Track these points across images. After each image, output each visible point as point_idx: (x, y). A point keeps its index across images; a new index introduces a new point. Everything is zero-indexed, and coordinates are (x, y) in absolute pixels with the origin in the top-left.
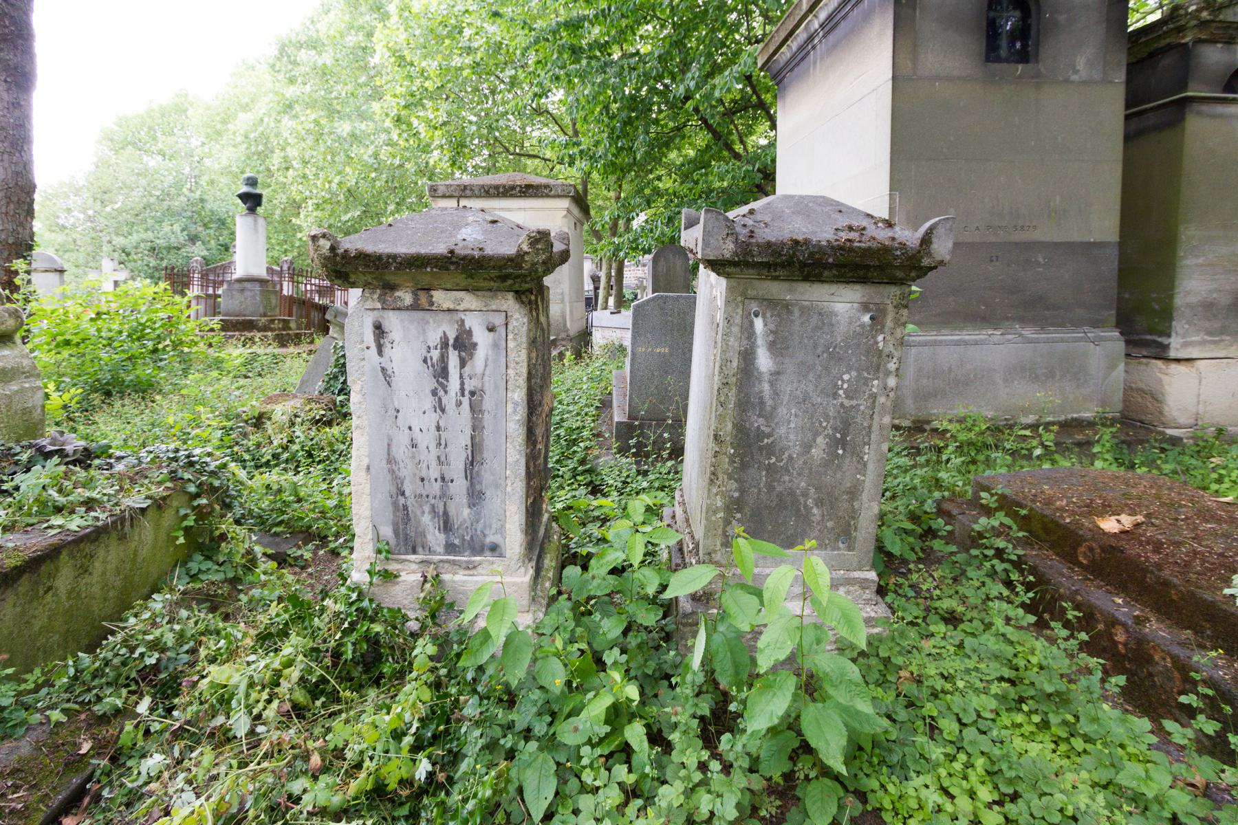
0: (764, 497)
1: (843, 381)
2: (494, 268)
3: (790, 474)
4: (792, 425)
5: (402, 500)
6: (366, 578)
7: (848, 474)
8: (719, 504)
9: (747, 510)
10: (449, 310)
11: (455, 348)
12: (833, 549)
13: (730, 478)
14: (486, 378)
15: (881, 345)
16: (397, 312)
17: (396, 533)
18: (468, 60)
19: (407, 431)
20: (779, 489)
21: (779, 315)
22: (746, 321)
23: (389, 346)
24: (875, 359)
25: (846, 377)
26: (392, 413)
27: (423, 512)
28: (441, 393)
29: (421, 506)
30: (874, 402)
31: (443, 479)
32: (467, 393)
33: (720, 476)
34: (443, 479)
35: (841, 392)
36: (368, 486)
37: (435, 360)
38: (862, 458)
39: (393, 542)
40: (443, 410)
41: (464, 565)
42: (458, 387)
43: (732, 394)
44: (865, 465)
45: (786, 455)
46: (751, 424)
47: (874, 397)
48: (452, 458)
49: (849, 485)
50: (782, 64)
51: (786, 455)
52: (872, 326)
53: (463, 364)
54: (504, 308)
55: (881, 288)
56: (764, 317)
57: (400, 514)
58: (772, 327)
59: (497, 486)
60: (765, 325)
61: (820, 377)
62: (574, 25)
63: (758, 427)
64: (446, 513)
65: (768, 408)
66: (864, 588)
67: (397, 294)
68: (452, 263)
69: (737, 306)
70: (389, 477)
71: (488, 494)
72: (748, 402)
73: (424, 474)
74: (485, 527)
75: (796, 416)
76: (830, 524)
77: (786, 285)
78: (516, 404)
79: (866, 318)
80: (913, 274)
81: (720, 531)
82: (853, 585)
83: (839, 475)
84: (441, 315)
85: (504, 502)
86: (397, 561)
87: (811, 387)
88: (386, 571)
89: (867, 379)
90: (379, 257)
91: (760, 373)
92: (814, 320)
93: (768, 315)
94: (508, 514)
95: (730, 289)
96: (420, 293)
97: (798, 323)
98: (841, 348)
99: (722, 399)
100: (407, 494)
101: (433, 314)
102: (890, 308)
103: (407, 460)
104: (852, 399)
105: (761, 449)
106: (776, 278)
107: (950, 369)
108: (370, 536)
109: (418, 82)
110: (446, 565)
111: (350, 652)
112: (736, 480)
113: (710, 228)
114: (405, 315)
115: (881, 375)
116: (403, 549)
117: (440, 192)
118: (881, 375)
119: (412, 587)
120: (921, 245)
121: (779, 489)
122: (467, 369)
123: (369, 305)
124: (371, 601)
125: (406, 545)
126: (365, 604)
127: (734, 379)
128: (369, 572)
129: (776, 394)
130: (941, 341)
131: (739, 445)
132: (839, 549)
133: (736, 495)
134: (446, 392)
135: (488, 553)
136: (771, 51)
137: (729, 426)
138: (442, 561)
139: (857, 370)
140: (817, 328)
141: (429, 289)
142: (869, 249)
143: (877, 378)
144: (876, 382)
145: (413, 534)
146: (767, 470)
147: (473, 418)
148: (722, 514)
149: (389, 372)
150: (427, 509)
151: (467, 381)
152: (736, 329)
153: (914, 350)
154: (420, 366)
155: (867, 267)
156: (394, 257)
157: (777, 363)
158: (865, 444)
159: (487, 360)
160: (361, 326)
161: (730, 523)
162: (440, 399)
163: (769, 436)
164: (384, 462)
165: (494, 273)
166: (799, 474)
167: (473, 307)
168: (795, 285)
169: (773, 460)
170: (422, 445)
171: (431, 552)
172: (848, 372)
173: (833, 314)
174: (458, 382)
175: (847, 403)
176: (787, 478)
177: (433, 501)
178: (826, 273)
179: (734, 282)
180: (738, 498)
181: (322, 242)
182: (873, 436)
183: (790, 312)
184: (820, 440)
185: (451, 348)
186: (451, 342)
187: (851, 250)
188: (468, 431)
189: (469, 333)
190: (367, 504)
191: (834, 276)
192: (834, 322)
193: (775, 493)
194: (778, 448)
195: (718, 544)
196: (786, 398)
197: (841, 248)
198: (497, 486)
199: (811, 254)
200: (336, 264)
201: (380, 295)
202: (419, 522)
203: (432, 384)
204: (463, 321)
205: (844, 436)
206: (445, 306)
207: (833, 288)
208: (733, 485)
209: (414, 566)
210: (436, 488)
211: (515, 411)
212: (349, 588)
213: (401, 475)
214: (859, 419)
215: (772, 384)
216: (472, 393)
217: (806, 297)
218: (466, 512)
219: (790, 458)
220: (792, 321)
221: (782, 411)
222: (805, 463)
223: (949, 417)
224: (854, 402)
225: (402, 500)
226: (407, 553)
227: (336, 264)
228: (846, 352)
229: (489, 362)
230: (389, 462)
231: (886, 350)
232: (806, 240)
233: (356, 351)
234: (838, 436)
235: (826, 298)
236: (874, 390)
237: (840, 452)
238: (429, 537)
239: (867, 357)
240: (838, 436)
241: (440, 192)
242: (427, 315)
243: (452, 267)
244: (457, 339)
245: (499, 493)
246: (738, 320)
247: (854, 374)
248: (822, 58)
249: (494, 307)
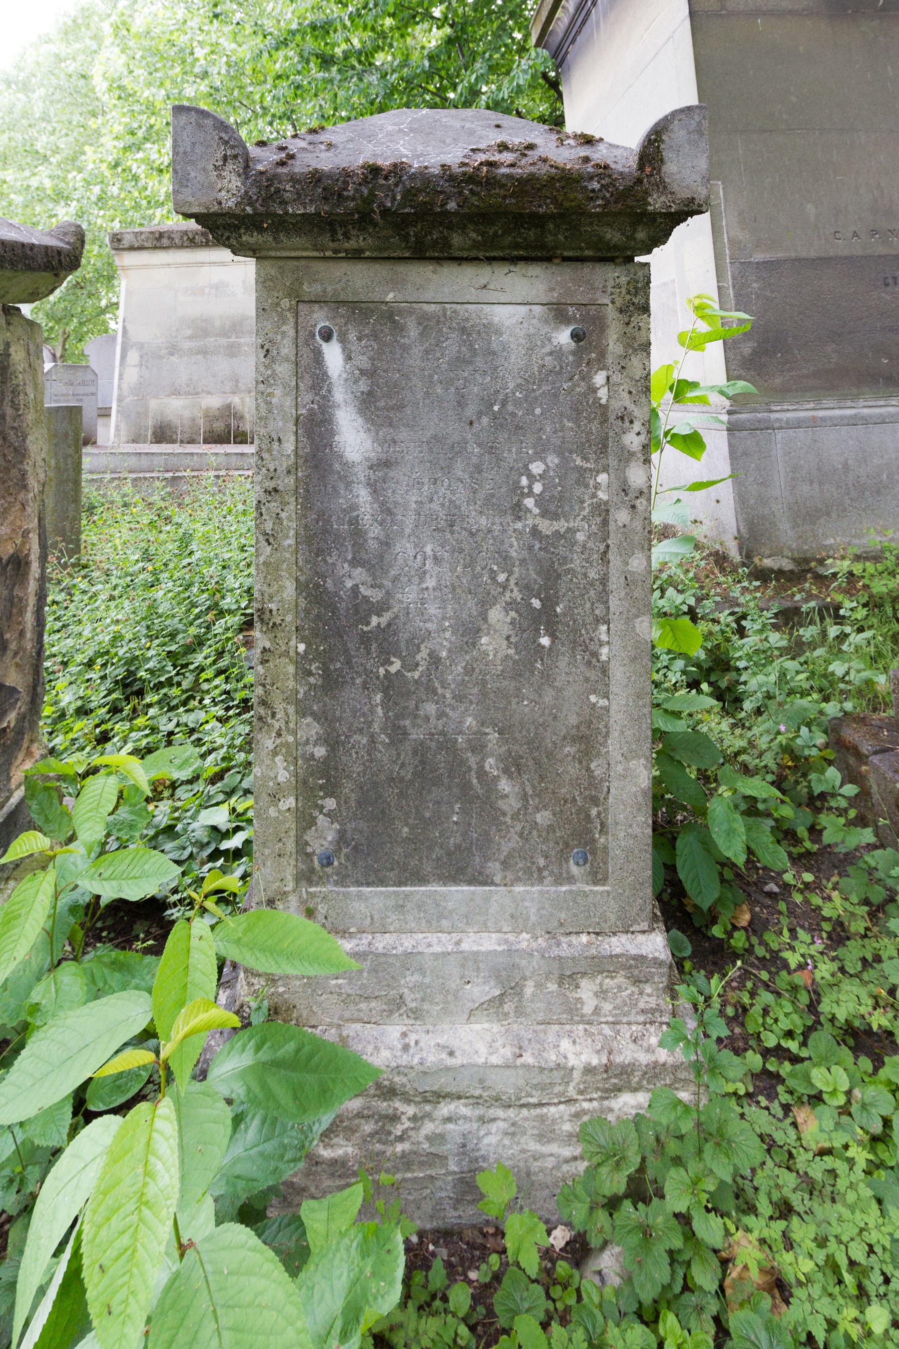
0: (384, 755)
1: (531, 478)
3: (440, 700)
4: (430, 583)
7: (568, 693)
8: (283, 776)
9: (347, 788)
12: (558, 881)
13: (302, 712)
15: (603, 394)
20: (417, 735)
21: (375, 336)
22: (305, 351)
24: (594, 426)
25: (537, 468)
30: (605, 523)
33: (279, 707)
35: (529, 502)
38: (595, 655)
43: (290, 513)
44: (605, 670)
45: (423, 654)
46: (339, 582)
47: (603, 512)
49: (573, 720)
51: (423, 654)
52: (578, 353)
55: (586, 270)
56: (343, 340)
58: (363, 361)
60: (348, 358)
61: (479, 469)
62: (322, 29)
63: (355, 589)
65: (372, 545)
66: (637, 981)
69: (283, 320)
72: (325, 531)
75: (437, 560)
76: (543, 818)
77: (382, 270)
79: (563, 337)
80: (641, 235)
81: (290, 845)
82: (611, 974)
83: (548, 697)
87: (461, 495)
89: (581, 471)
91: (348, 466)
92: (452, 345)
93: (352, 336)
95: (264, 283)
97: (417, 351)
98: (517, 403)
99: (268, 526)
102: (611, 313)
104: (555, 517)
105: (365, 639)
106: (356, 256)
107: (846, 467)
112: (314, 715)
113: (186, 145)
115: (613, 462)
117: (126, 243)
118: (613, 462)
120: (641, 167)
121: (417, 735)
127: (291, 480)
129: (386, 511)
130: (823, 419)
131: (315, 633)
132: (571, 879)
133: (320, 752)
136: (544, 19)
137: (289, 589)
139: (560, 452)
140: (460, 361)
142: (532, 178)
143: (605, 469)
144: (603, 478)
146: (385, 691)
148: (290, 802)
152: (284, 370)
153: (780, 435)
155: (538, 221)
157: (382, 442)
158: (598, 621)
161: (312, 822)
163: (380, 608)
166: (459, 698)
168: (402, 269)
169: (396, 666)
172: (539, 456)
173: (491, 329)
175: (546, 527)
176: (430, 708)
178: (456, 239)
179: (271, 269)
180: (327, 759)
182: (614, 603)
183: (398, 329)
184: (496, 615)
187: (492, 182)
191: (476, 245)
192: (495, 346)
193: (408, 747)
194: (404, 636)
195: (289, 874)
196: (409, 522)
197: (471, 178)
199: (409, 194)
205: (549, 603)
207: (483, 274)
208: (311, 728)
214: (577, 563)
215: (375, 488)
217: (428, 296)
219: (434, 660)
220: (405, 348)
221: (404, 548)
222: (469, 670)
223: (856, 550)
224: (561, 525)
228: (530, 411)
231: (616, 406)
232: (395, 165)
234: (536, 603)
235: (472, 294)
236: (602, 495)
237: (545, 641)
239: (577, 421)
240: (536, 603)
241: (126, 243)
246: (287, 349)
247: (553, 460)
248: (605, 15)
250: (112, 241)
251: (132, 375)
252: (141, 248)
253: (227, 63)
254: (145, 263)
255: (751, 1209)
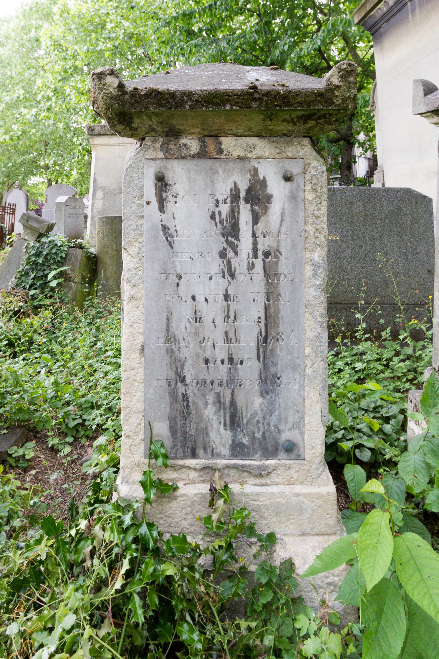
2: (301, 104)
5: (181, 388)
6: (140, 493)
10: (239, 158)
11: (247, 201)
14: (282, 236)
16: (182, 161)
17: (173, 430)
18: (109, 45)
19: (190, 301)
23: (172, 200)
26: (173, 279)
27: (206, 404)
28: (230, 254)
29: (204, 395)
31: (231, 360)
32: (260, 253)
34: (231, 360)
36: (142, 371)
37: (224, 215)
39: (168, 443)
40: (232, 275)
41: (256, 472)
42: (250, 246)
48: (242, 334)
50: (378, 16)
53: (256, 219)
54: (301, 154)
57: (178, 406)
59: (294, 368)
64: (233, 404)
67: (182, 141)
68: (255, 99)
70: (167, 359)
71: (284, 378)
73: (208, 354)
74: (279, 420)
78: (316, 265)
84: (231, 164)
85: (302, 387)
86: (175, 468)
88: (160, 481)
90: (172, 95)
94: (307, 402)
96: (207, 139)
100: (188, 380)
101: (223, 163)
103: (189, 338)
108: (141, 436)
109: (70, 63)
110: (233, 472)
111: (140, 611)
114: (192, 164)
116: (180, 451)
117: (96, 132)
119: (193, 504)
122: (261, 226)
123: (150, 154)
124: (150, 525)
125: (184, 446)
126: (144, 529)
128: (143, 484)
134: (236, 253)
135: (282, 455)
136: (368, 8)
138: (228, 467)
141: (217, 136)
145: (193, 432)
147: (268, 283)
149: (172, 231)
150: (211, 398)
151: (260, 240)
154: (208, 224)
156: (189, 94)
159: (283, 214)
160: (142, 178)
162: (229, 262)
164: (162, 340)
165: (301, 111)
167: (266, 155)
170: (207, 320)
171: (214, 455)
174: (251, 241)
177: (218, 389)
181: (109, 79)
185: (242, 202)
186: (243, 194)
188: (261, 300)
189: (264, 183)
190: (139, 394)
198: (294, 368)
200: (123, 104)
201: (163, 143)
202: (200, 416)
203: (221, 244)
204: (256, 170)
206: (235, 154)
209: (193, 475)
210: (224, 369)
211: (315, 276)
212: (117, 507)
213: (182, 356)
216: (267, 254)
218: (258, 401)
225: (181, 388)
226: (185, 457)
227: (123, 104)
229: (285, 218)
230: (168, 340)
233: (134, 207)
238: (213, 436)
241: (96, 132)
242: (216, 164)
243: (254, 105)
244: (249, 191)
245: (297, 376)
249: (289, 154)
250: (88, 131)
251: (99, 204)
252: (105, 135)
253: (123, 33)
254: (106, 142)
255: (79, 389)
